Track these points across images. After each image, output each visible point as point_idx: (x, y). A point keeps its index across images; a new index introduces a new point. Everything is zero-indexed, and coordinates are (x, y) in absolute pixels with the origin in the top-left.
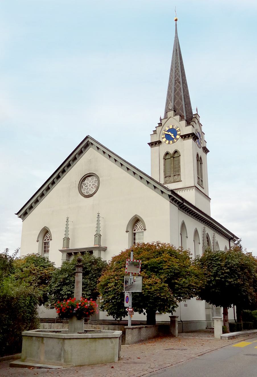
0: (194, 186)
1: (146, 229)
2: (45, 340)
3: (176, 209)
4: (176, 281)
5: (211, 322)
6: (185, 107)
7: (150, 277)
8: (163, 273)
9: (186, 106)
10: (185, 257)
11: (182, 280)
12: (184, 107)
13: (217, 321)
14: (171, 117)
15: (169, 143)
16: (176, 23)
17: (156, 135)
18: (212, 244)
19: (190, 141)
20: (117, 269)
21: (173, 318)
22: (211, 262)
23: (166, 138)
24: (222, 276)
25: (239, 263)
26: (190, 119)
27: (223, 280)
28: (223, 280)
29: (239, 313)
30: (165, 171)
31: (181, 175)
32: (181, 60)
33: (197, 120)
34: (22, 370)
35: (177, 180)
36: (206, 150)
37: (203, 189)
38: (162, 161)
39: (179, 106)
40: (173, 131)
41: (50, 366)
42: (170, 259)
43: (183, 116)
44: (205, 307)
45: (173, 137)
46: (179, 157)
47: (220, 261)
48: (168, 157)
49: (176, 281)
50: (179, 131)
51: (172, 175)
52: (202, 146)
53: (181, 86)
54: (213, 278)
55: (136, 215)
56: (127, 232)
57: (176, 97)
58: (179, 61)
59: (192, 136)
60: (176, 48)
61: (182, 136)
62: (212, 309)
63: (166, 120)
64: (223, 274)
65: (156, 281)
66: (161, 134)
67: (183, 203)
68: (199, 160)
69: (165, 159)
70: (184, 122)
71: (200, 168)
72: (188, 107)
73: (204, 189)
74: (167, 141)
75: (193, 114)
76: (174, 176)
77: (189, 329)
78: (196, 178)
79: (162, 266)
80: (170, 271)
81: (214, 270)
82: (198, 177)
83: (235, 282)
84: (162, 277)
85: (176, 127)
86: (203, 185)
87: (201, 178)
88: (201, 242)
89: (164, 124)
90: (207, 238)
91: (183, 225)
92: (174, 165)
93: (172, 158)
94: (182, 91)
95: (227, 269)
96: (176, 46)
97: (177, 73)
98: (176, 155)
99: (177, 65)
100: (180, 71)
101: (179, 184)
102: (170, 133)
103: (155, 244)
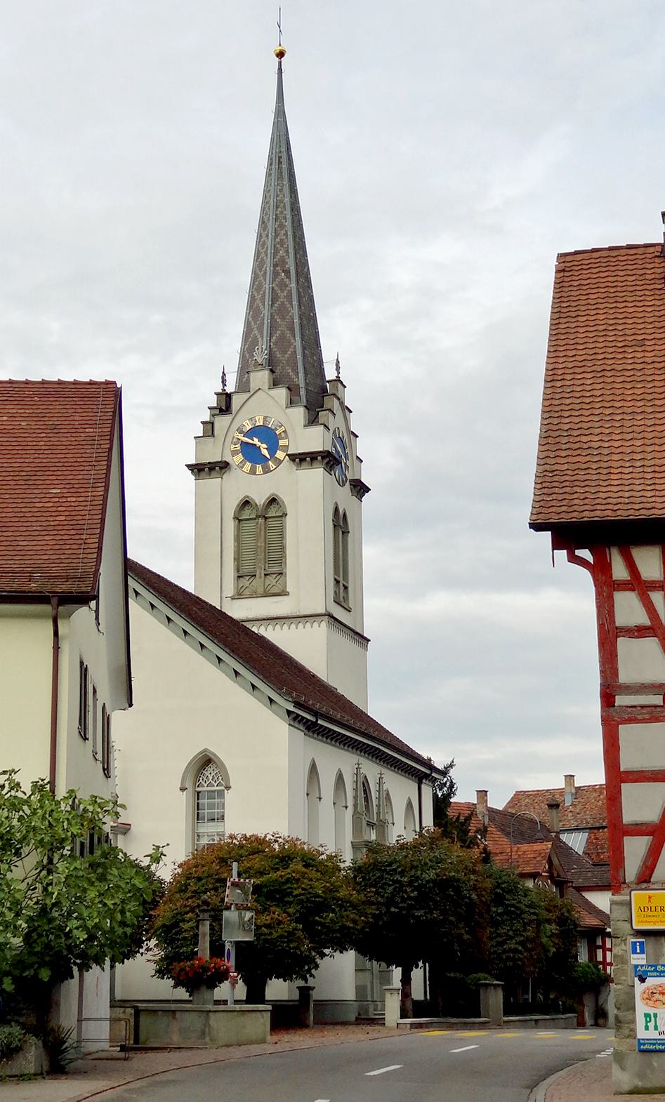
0: (325, 615)
1: (231, 785)
2: (178, 1015)
3: (300, 735)
4: (317, 918)
5: (368, 1005)
6: (304, 356)
8: (290, 903)
9: (306, 352)
11: (328, 916)
12: (299, 357)
13: (391, 994)
14: (259, 389)
15: (253, 472)
17: (211, 439)
18: (375, 802)
19: (316, 475)
20: (195, 892)
21: (305, 992)
22: (382, 876)
23: (243, 455)
24: (403, 905)
25: (437, 877)
26: (319, 397)
27: (404, 912)
28: (404, 912)
29: (434, 981)
30: (237, 559)
31: (285, 576)
33: (339, 399)
35: (275, 590)
36: (360, 489)
37: (348, 612)
38: (230, 526)
40: (268, 434)
42: (306, 873)
45: (265, 452)
46: (282, 516)
47: (400, 873)
48: (247, 514)
49: (317, 918)
51: (261, 574)
52: (350, 477)
53: (293, 285)
54: (384, 909)
55: (205, 750)
56: (183, 789)
58: (287, 200)
59: (323, 458)
61: (292, 457)
62: (371, 971)
63: (246, 396)
64: (404, 900)
65: (280, 918)
66: (229, 439)
67: (317, 721)
68: (341, 524)
69: (238, 520)
70: (299, 413)
71: (343, 547)
72: (313, 354)
73: (350, 611)
74: (248, 465)
75: (327, 379)
76: (265, 575)
78: (331, 583)
79: (292, 888)
80: (307, 898)
81: (387, 893)
82: (335, 579)
83: (429, 916)
84: (291, 910)
85: (276, 423)
86: (348, 599)
87: (344, 580)
88: (350, 803)
89: (239, 410)
90: (365, 791)
91: (313, 769)
92: (265, 543)
93: (261, 520)
94: (295, 303)
95: (412, 892)
96: (280, 147)
98: (272, 512)
100: (290, 233)
101: (277, 602)
102: (256, 441)
103: (269, 837)
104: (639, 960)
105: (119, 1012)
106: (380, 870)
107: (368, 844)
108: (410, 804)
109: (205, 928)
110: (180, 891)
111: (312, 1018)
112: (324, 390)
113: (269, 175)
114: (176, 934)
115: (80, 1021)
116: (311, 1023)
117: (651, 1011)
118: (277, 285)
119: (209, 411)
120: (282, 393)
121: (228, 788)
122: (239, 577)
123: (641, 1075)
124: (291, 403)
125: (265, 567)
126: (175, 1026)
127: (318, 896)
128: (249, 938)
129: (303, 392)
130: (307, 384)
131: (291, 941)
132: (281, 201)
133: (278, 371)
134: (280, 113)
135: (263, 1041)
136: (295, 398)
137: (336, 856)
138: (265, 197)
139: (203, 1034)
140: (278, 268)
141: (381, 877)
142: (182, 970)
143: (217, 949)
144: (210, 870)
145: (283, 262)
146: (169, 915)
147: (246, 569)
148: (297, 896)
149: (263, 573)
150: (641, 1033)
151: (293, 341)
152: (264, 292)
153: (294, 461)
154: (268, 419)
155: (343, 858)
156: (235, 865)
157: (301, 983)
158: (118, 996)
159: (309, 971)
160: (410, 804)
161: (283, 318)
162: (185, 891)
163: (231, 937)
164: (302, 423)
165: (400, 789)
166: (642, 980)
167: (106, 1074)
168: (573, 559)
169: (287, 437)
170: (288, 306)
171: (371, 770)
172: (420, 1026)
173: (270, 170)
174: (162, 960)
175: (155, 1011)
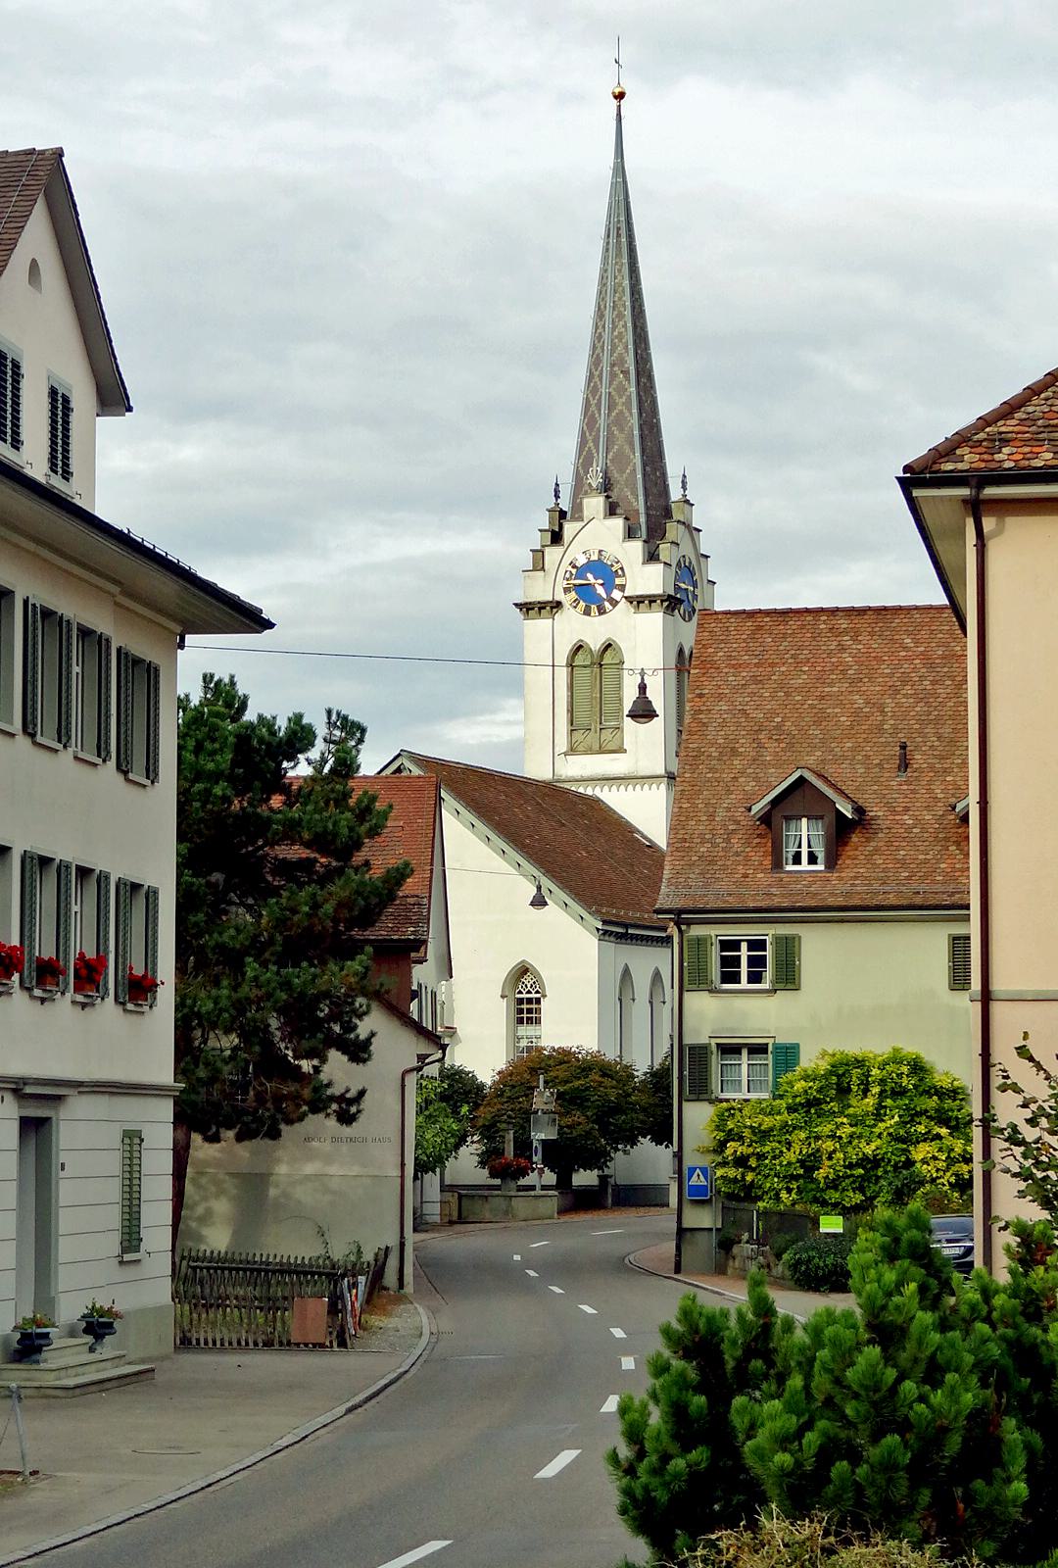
3: (610, 946)
4: (611, 1120)
7: (568, 1113)
9: (648, 469)
10: (628, 1073)
15: (587, 612)
20: (509, 1097)
21: (603, 1179)
30: (571, 711)
31: (623, 732)
32: (634, 275)
34: (454, 1242)
38: (562, 674)
39: (622, 471)
40: (605, 570)
41: (422, 1238)
42: (603, 1082)
45: (601, 591)
49: (611, 1120)
50: (620, 576)
53: (633, 389)
55: (523, 961)
57: (613, 433)
58: (626, 282)
60: (619, 221)
61: (630, 599)
69: (571, 665)
70: (637, 547)
72: (655, 470)
91: (626, 973)
94: (635, 411)
97: (620, 333)
99: (620, 299)
105: (448, 1196)
114: (494, 1132)
115: (422, 1203)
116: (610, 1205)
118: (614, 389)
119: (539, 533)
120: (618, 524)
121: (544, 996)
122: (572, 730)
124: (630, 534)
125: (601, 719)
126: (487, 1206)
128: (554, 1136)
129: (643, 519)
130: (647, 508)
131: (589, 1139)
132: (620, 285)
134: (620, 170)
135: (551, 1218)
137: (631, 1066)
140: (616, 369)
143: (524, 1146)
144: (534, 1068)
145: (622, 361)
146: (489, 1117)
148: (594, 1102)
149: (598, 726)
151: (632, 457)
152: (629, 397)
153: (631, 603)
154: (603, 553)
158: (447, 1182)
159: (605, 1163)
161: (622, 430)
162: (501, 1095)
167: (438, 1231)
169: (624, 576)
170: (627, 414)
173: (608, 243)
175: (473, 1196)
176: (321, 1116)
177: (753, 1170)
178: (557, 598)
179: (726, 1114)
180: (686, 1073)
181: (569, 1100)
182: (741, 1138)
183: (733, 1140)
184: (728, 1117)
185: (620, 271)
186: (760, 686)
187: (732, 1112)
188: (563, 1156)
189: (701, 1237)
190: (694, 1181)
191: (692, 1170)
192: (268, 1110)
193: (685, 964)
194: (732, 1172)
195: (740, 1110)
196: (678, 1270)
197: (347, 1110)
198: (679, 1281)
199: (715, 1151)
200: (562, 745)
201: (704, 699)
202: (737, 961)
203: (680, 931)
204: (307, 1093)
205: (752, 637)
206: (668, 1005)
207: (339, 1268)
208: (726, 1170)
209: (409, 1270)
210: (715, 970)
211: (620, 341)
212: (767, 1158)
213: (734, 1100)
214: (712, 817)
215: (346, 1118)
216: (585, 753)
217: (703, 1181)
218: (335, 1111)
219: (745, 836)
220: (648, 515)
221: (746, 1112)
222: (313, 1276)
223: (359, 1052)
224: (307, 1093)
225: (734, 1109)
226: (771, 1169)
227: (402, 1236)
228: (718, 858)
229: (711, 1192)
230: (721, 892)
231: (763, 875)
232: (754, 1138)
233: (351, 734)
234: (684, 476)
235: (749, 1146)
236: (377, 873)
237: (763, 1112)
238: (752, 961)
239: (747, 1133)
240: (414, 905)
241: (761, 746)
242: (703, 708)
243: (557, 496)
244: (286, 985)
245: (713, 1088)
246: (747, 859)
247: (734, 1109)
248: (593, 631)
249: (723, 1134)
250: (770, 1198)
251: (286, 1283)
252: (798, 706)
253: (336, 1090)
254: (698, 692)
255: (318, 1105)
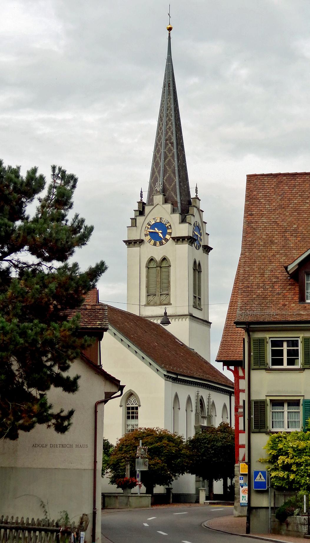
3: (170, 383)
6: (180, 186)
12: (178, 187)
15: (155, 244)
16: (169, 34)
17: (135, 228)
18: (206, 407)
20: (125, 451)
21: (169, 490)
26: (186, 206)
30: (147, 287)
35: (165, 302)
36: (207, 249)
38: (144, 270)
43: (177, 202)
44: (195, 480)
45: (161, 235)
48: (152, 265)
52: (202, 244)
53: (175, 150)
55: (130, 390)
56: (121, 406)
58: (172, 106)
59: (188, 239)
60: (169, 81)
61: (174, 239)
66: (144, 228)
69: (148, 268)
70: (177, 217)
75: (192, 197)
77: (181, 499)
84: (163, 459)
91: (176, 396)
93: (159, 268)
94: (176, 159)
97: (170, 127)
98: (164, 264)
99: (170, 113)
104: (241, 482)
106: (200, 442)
107: (203, 428)
108: (225, 406)
109: (128, 467)
110: (119, 450)
111: (171, 500)
112: (190, 203)
113: (164, 93)
117: (244, 495)
120: (169, 206)
121: (140, 406)
123: (241, 512)
124: (174, 211)
127: (173, 453)
129: (179, 205)
130: (181, 201)
132: (170, 107)
133: (167, 194)
134: (169, 60)
135: (148, 507)
136: (176, 208)
138: (162, 104)
139: (127, 504)
141: (200, 445)
142: (120, 482)
143: (133, 473)
144: (133, 439)
145: (170, 138)
147: (152, 291)
150: (241, 501)
152: (173, 154)
153: (174, 240)
155: (184, 438)
156: (141, 441)
157: (167, 487)
159: (170, 482)
160: (225, 406)
161: (170, 168)
162: (121, 450)
163: (138, 470)
164: (178, 222)
165: (220, 400)
166: (242, 487)
168: (228, 369)
169: (171, 228)
171: (204, 393)
172: (214, 504)
173: (164, 90)
174: (112, 477)
176: (45, 425)
177: (294, 472)
178: (142, 238)
179: (277, 440)
180: (253, 416)
181: (153, 453)
182: (287, 454)
183: (282, 455)
184: (278, 442)
185: (169, 101)
186: (284, 210)
187: (280, 439)
188: (150, 480)
189: (262, 513)
190: (258, 479)
191: (256, 473)
192: (10, 419)
193: (252, 354)
194: (281, 474)
195: (285, 438)
196: (248, 531)
197: (62, 423)
198: (250, 537)
199: (270, 462)
200: (144, 302)
201: (253, 217)
202: (281, 353)
203: (249, 336)
204: (36, 408)
205: (277, 186)
206: (194, 412)
207: (60, 527)
208: (277, 472)
209: (98, 530)
210: (269, 358)
211: (170, 130)
212: (302, 466)
213: (281, 432)
214: (262, 275)
215: (61, 428)
216: (154, 305)
217: (263, 480)
218: (53, 424)
219: (282, 285)
220: (181, 203)
221: (289, 438)
222: (35, 532)
223: (71, 386)
224: (36, 408)
225: (281, 437)
226: (305, 472)
227: (94, 508)
228: (268, 296)
229: (268, 485)
230: (272, 313)
231: (294, 305)
232: (295, 454)
233: (67, 183)
234: (197, 188)
235: (291, 458)
236: (83, 269)
237: (299, 439)
238: (289, 353)
239: (290, 451)
240: (100, 309)
241: (286, 239)
242: (253, 221)
243: (141, 197)
244: (23, 334)
245: (268, 425)
246: (284, 296)
247: (281, 437)
248: (158, 253)
249: (276, 451)
250: (304, 489)
251: (20, 538)
252: (306, 220)
253: (55, 411)
254: (249, 213)
255: (43, 418)
